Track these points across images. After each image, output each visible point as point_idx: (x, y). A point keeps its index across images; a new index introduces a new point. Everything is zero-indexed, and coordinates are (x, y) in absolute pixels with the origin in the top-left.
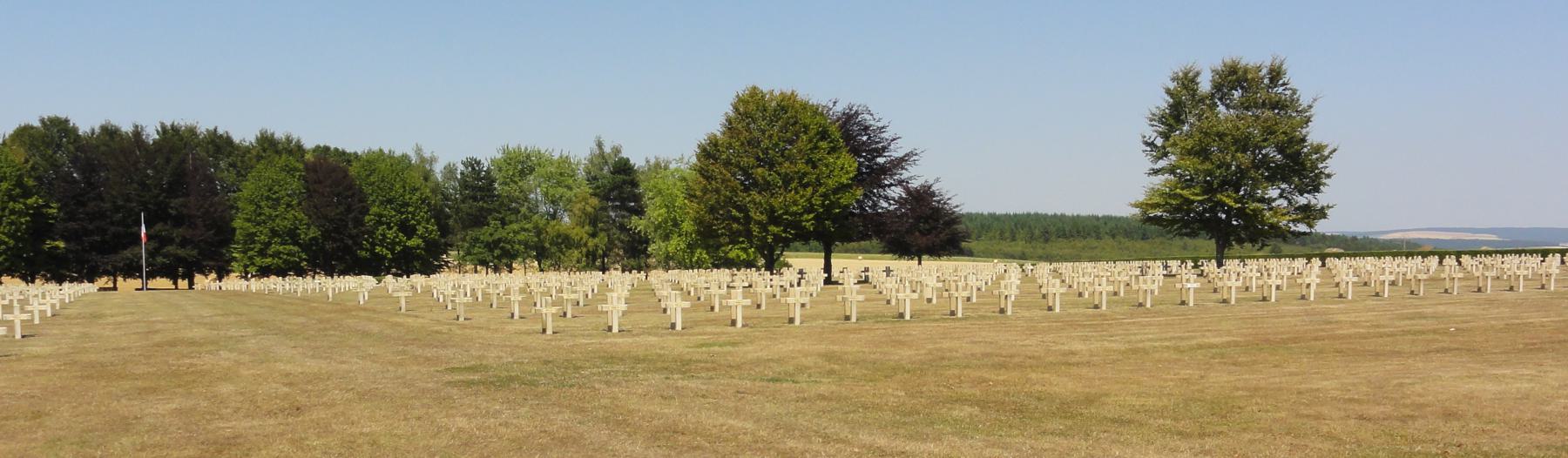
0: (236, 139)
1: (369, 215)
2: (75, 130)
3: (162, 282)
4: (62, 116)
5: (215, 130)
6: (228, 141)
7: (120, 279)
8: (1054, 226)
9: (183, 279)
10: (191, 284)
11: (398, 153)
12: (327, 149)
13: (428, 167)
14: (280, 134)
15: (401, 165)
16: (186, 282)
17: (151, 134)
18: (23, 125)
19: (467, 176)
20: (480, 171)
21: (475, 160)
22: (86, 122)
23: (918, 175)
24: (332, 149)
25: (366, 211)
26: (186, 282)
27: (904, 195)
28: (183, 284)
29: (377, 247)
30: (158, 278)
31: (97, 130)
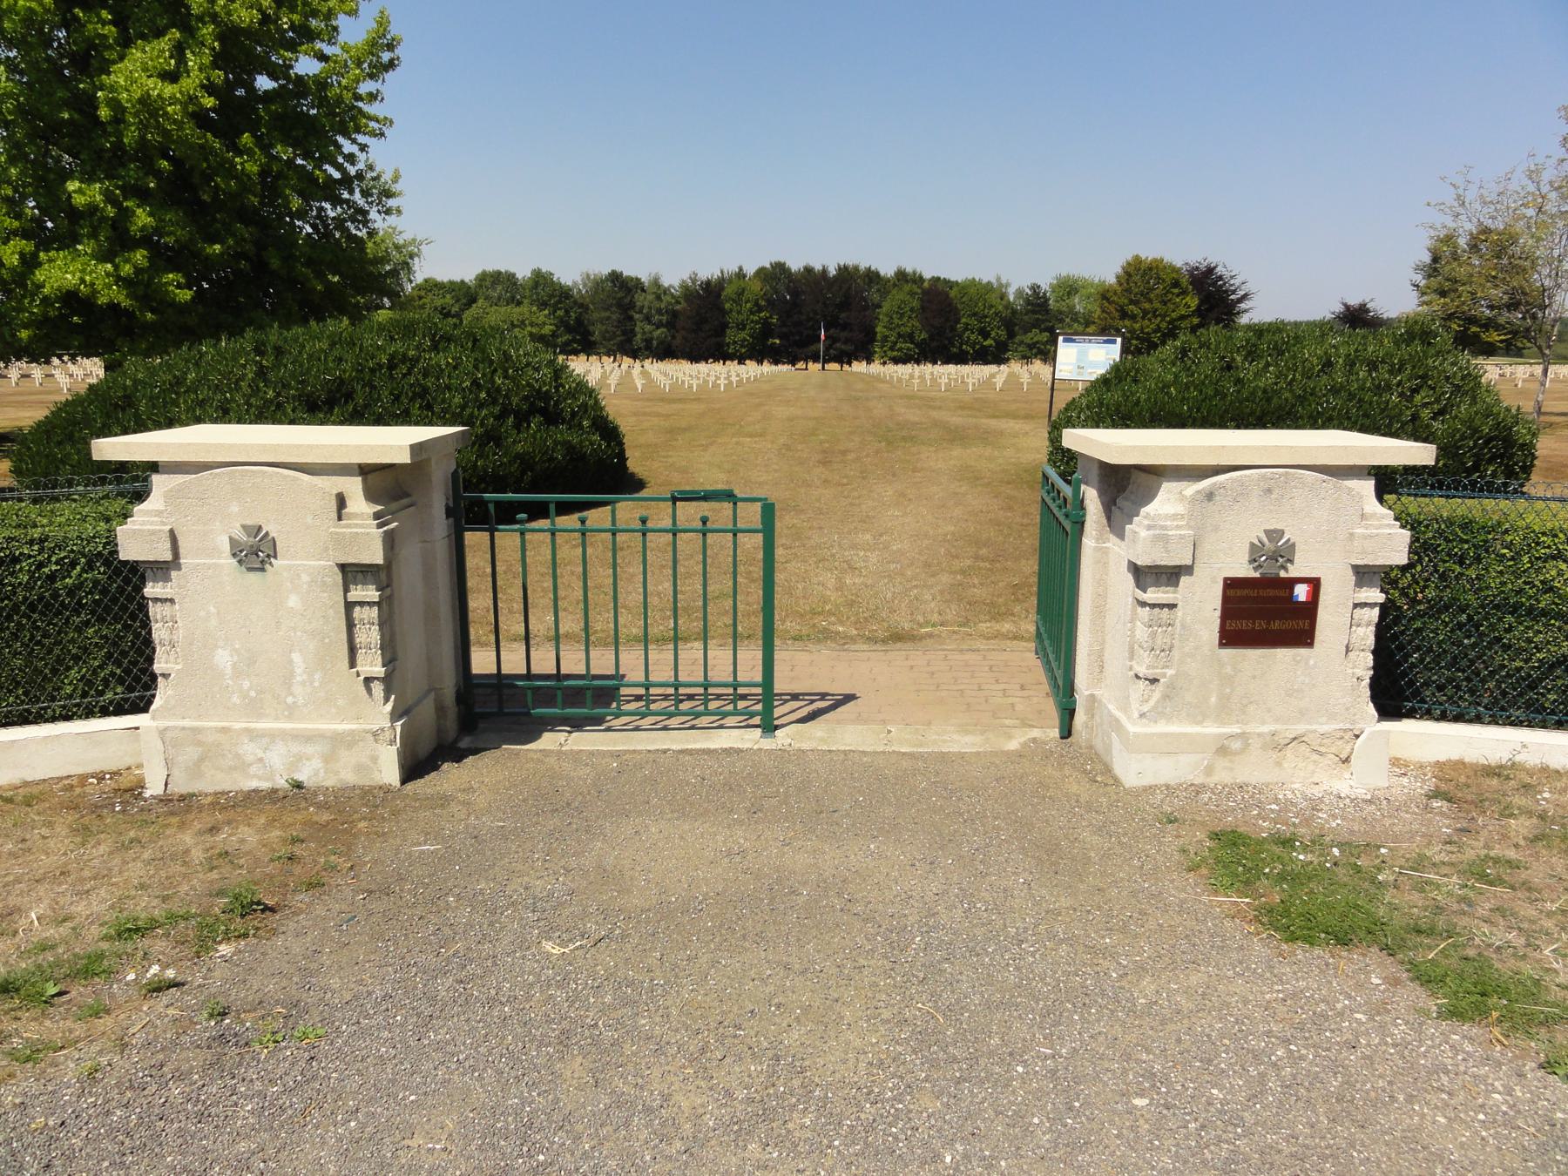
0: (882, 273)
6: (877, 274)
12: (939, 278)
14: (909, 270)
15: (988, 287)
22: (795, 265)
23: (750, 270)
25: (958, 321)
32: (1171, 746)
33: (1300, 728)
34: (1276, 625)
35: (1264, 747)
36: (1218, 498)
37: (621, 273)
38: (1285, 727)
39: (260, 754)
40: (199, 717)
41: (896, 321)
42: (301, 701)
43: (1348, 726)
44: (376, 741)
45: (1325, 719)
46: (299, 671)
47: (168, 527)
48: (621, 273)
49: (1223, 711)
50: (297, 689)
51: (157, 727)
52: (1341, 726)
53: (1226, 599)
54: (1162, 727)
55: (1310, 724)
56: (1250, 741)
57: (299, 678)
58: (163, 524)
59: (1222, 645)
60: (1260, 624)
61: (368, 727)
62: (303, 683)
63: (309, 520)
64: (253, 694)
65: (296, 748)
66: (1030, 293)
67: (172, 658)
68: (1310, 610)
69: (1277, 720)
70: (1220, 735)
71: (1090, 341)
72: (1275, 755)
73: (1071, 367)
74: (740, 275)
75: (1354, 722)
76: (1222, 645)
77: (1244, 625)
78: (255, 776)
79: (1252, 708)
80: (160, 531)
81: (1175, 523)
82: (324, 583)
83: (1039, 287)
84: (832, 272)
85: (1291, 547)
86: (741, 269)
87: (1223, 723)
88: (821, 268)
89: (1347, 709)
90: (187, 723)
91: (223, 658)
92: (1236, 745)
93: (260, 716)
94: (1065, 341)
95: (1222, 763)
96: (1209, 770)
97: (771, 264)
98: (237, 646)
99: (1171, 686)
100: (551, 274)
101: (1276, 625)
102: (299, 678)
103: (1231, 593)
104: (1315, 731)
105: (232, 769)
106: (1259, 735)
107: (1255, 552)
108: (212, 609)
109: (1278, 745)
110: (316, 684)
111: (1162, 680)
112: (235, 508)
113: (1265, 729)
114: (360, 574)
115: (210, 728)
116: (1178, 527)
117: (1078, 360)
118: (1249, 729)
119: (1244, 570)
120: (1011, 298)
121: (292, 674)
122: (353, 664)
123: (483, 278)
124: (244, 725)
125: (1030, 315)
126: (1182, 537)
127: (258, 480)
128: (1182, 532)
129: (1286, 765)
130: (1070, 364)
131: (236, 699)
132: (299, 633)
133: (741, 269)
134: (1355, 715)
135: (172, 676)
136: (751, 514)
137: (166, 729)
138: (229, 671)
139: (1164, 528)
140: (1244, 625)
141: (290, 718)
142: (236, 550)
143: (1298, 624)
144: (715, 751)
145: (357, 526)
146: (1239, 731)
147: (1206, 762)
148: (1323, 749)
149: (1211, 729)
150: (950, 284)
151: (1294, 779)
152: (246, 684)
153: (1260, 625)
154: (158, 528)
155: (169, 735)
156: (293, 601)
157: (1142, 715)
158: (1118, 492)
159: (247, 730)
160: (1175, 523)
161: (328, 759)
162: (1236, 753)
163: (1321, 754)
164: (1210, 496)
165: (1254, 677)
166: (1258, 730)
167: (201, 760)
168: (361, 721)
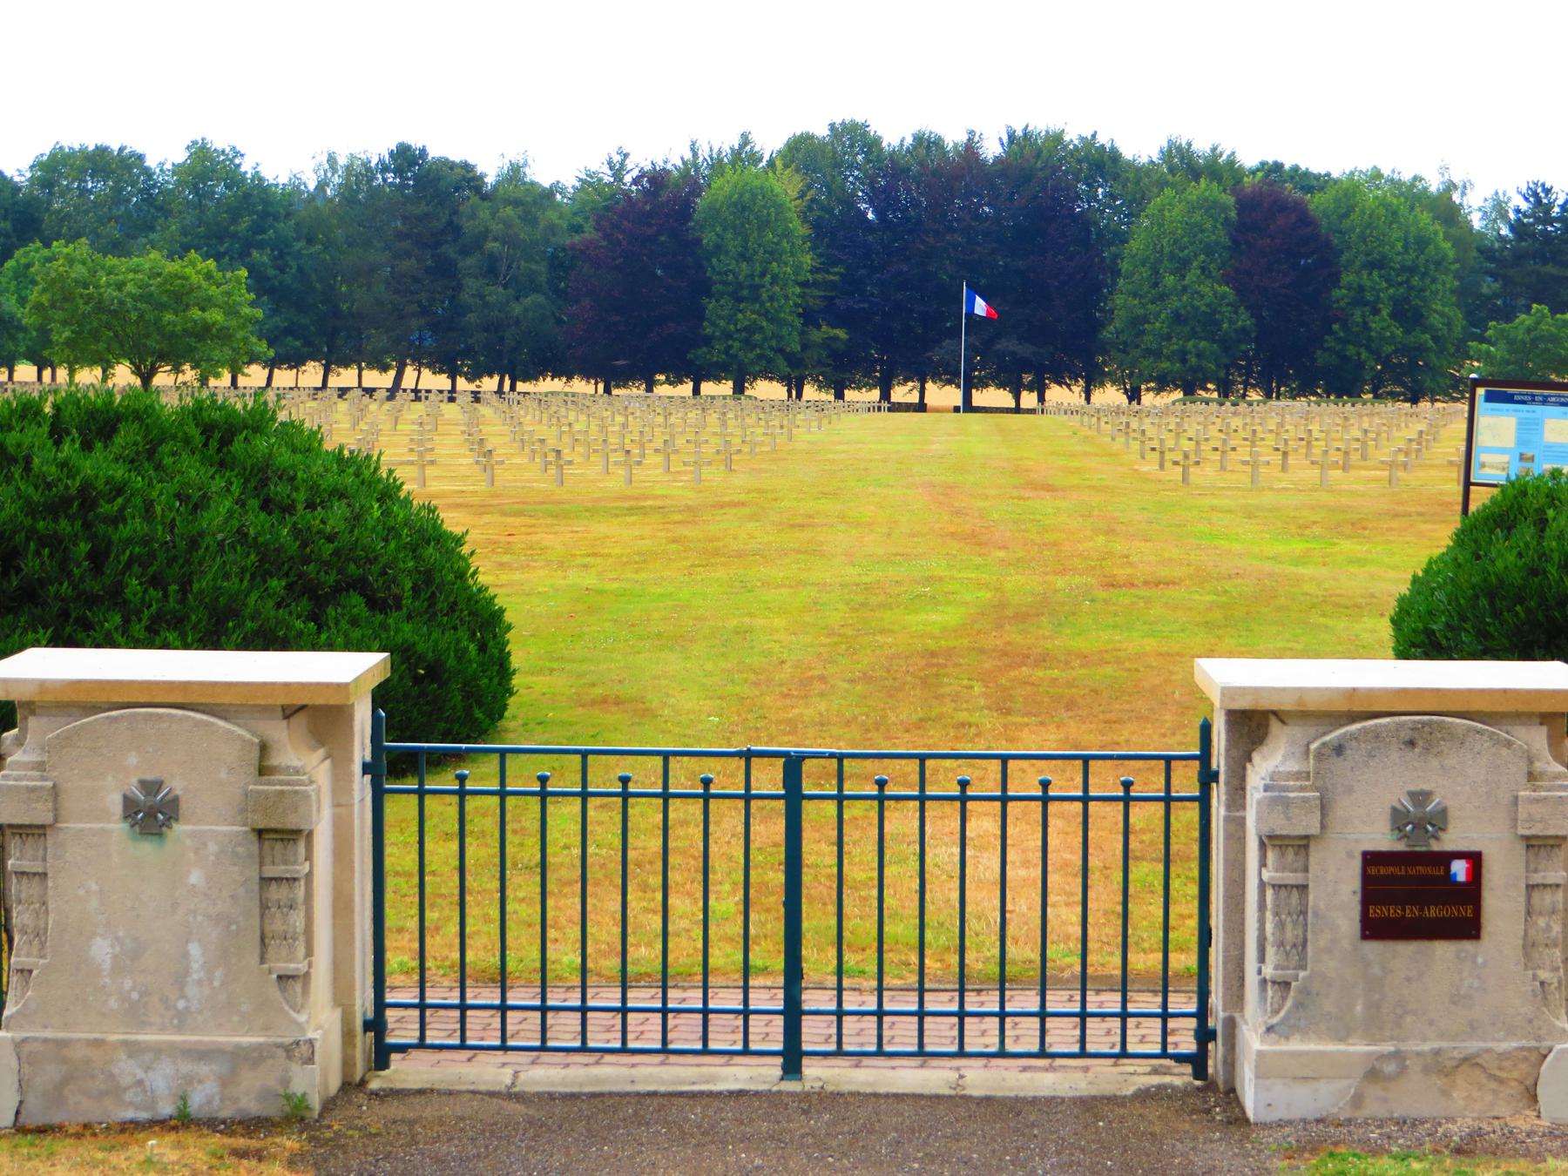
0: (1128, 153)
1: (1340, 288)
2: (877, 141)
3: (768, 390)
4: (860, 119)
5: (1094, 136)
6: (1115, 156)
7: (929, 385)
8: (310, 241)
9: (1031, 390)
10: (1041, 399)
11: (1406, 176)
12: (1278, 167)
13: (1456, 197)
14: (1202, 147)
15: (1412, 194)
16: (1035, 395)
17: (991, 149)
18: (798, 133)
19: (1525, 215)
20: (1550, 206)
21: (1543, 185)
22: (894, 133)
23: (770, 143)
24: (1287, 167)
25: (1335, 279)
26: (1035, 395)
27: (249, 176)
28: (1029, 399)
29: (1351, 347)
30: (991, 389)
31: (909, 141)
32: (1306, 1072)
33: (1473, 1045)
34: (1433, 912)
35: (1426, 1070)
36: (1348, 752)
37: (423, 151)
38: (1453, 1044)
39: (140, 1074)
40: (66, 1026)
41: (1170, 280)
42: (194, 1006)
43: (1533, 1043)
44: (289, 1057)
45: (1502, 1033)
46: (195, 966)
47: (50, 784)
48: (423, 151)
49: (1373, 1026)
50: (191, 991)
51: (13, 1039)
52: (1524, 1043)
53: (1366, 879)
54: (1295, 1045)
55: (1485, 1040)
56: (1408, 1062)
57: (195, 976)
58: (44, 779)
59: (1364, 937)
60: (1411, 911)
61: (279, 1040)
62: (200, 982)
63: (223, 775)
64: (135, 996)
65: (186, 1067)
66: (1524, 206)
67: (35, 950)
68: (1472, 892)
69: (1441, 1036)
70: (1369, 1054)
71: (1545, 401)
72: (1440, 1082)
73: (1505, 458)
74: (743, 155)
75: (1539, 1038)
76: (1364, 937)
77: (1392, 911)
78: (131, 1103)
79: (1409, 1019)
80: (42, 787)
81: (1298, 783)
82: (235, 854)
83: (1548, 191)
84: (991, 149)
85: (1443, 813)
86: (745, 140)
87: (1373, 1042)
88: (965, 138)
89: (1530, 1021)
90: (48, 1034)
91: (102, 950)
92: (1390, 1068)
93: (143, 1025)
94: (1490, 398)
95: (1374, 1091)
96: (1357, 1101)
97: (832, 126)
98: (121, 934)
99: (1305, 991)
100: (238, 154)
101: (1433, 912)
102: (195, 976)
103: (1372, 871)
104: (1488, 1051)
105: (104, 1094)
106: (1419, 1054)
107: (1398, 819)
108: (94, 887)
109: (1441, 1067)
110: (216, 984)
111: (1294, 984)
112: (132, 759)
113: (1426, 1047)
114: (279, 843)
115: (79, 1040)
116: (1302, 789)
117: (1521, 441)
118: (1403, 1047)
119: (1384, 840)
120: (1477, 222)
121: (187, 972)
122: (263, 960)
123: (54, 168)
124: (122, 1037)
125: (1531, 265)
126: (1305, 800)
127: (165, 725)
128: (1307, 794)
129: (1455, 1095)
130: (1502, 451)
131: (113, 1003)
132: (200, 918)
133: (745, 140)
134: (1540, 1028)
135: (35, 973)
136: (769, 778)
137: (25, 1040)
138: (107, 966)
139: (1286, 789)
140: (1392, 911)
141: (179, 1029)
142: (130, 808)
143: (1459, 911)
144: (721, 1093)
145: (282, 783)
146: (1392, 1049)
147: (1352, 1091)
148: (1503, 1075)
149: (1360, 1048)
150: (1309, 182)
151: (1467, 1113)
152: (128, 984)
153: (1411, 912)
154: (38, 783)
155: (27, 1048)
156: (195, 877)
157: (1270, 1029)
158: (1253, 744)
159: (125, 1043)
160: (1298, 783)
161: (225, 1082)
162: (1389, 1078)
163: (1501, 1081)
164: (1339, 750)
165: (1409, 979)
166: (1418, 1048)
167: (66, 1081)
168: (269, 1033)
